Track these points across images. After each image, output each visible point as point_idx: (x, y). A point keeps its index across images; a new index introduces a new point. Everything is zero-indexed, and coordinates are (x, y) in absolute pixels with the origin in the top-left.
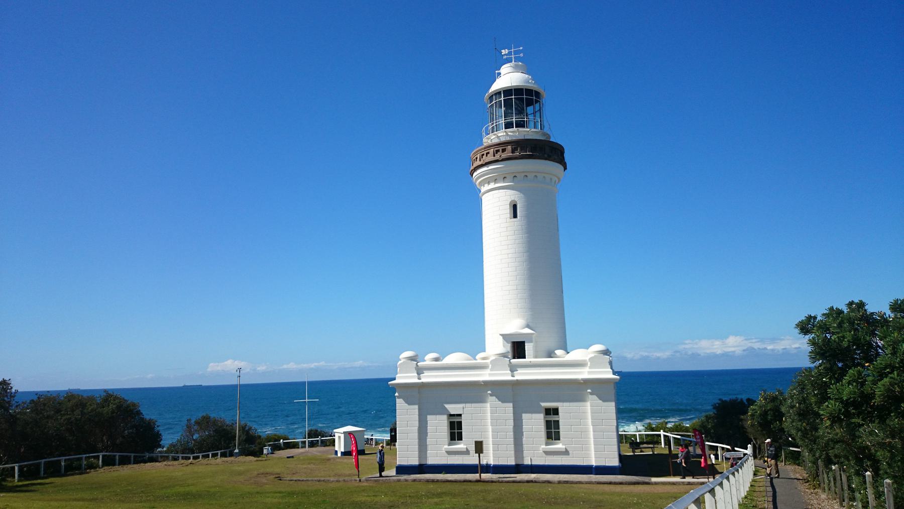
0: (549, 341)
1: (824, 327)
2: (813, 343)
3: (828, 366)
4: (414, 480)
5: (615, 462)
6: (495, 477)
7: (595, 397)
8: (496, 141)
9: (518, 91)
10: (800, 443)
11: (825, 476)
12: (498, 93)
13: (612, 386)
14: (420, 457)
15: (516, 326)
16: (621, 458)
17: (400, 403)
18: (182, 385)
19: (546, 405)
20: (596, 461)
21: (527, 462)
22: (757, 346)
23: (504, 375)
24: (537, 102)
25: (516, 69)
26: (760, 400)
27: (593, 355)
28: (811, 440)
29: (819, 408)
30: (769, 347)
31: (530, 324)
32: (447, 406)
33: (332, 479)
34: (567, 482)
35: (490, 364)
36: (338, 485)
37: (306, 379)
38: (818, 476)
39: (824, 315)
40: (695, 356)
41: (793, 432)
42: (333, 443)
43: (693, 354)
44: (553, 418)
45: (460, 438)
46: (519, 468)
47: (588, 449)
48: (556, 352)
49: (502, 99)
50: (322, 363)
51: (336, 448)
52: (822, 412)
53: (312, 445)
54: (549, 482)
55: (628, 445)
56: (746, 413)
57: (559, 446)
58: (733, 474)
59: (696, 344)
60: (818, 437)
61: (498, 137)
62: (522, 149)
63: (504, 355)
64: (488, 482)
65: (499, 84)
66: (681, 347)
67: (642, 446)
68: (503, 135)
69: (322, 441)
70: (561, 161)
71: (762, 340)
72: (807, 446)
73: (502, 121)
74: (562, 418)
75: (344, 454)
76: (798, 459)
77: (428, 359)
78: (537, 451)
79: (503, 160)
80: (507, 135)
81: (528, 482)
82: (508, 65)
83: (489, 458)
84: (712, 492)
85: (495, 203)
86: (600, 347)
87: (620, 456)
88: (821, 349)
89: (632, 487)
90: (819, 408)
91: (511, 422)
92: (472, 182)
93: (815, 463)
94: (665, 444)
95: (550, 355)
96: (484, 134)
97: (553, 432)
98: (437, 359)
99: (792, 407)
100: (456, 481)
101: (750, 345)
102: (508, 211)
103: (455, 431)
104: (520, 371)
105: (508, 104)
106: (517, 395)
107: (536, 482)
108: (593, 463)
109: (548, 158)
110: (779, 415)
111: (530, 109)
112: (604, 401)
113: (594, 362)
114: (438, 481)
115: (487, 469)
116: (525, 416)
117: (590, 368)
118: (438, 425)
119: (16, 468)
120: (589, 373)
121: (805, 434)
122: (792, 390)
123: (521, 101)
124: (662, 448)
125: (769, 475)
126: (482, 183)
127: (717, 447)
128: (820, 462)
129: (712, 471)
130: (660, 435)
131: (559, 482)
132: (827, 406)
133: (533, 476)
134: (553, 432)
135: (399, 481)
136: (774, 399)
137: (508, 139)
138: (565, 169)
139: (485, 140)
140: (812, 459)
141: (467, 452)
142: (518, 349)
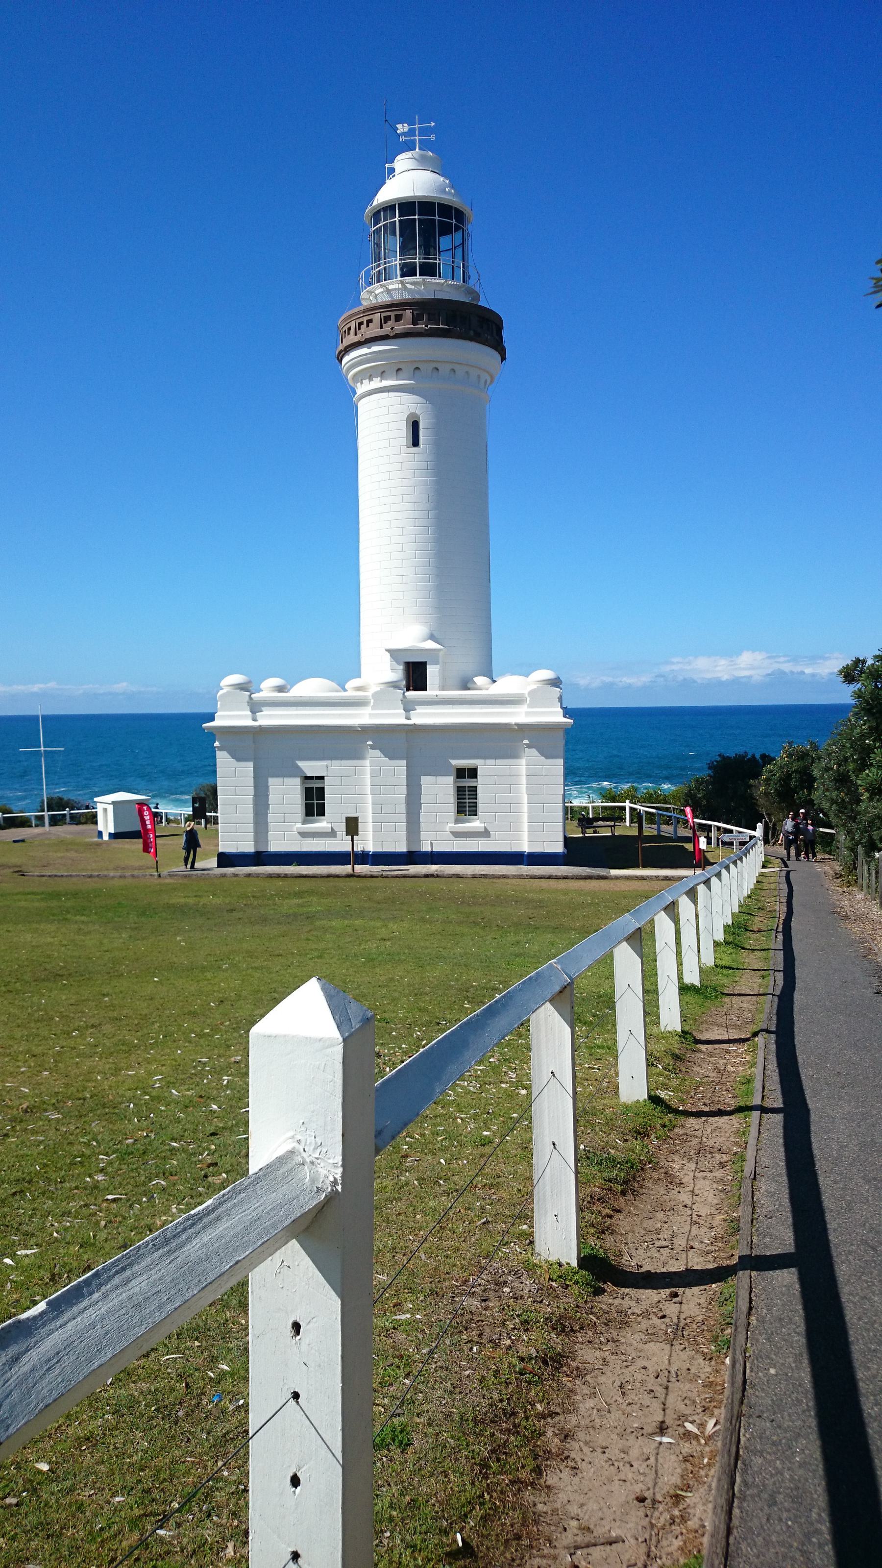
0: (464, 662)
1: (875, 674)
2: (859, 695)
3: (874, 724)
4: (249, 875)
5: (558, 847)
6: (376, 869)
7: (534, 751)
8: (384, 299)
9: (425, 206)
10: (834, 820)
11: (866, 867)
12: (389, 208)
13: (561, 734)
14: (256, 841)
15: (413, 636)
16: (567, 841)
17: (223, 758)
19: (459, 763)
20: (529, 846)
21: (426, 847)
22: (787, 667)
23: (395, 717)
24: (457, 228)
25: (423, 163)
26: (781, 757)
27: (535, 687)
28: (850, 817)
29: (857, 776)
30: (808, 671)
31: (435, 633)
32: (301, 764)
33: (112, 874)
34: (485, 876)
35: (371, 695)
36: (122, 882)
37: (39, 710)
38: (855, 868)
39: (876, 657)
40: (687, 684)
41: (826, 805)
42: (93, 819)
43: (685, 679)
44: (468, 782)
45: (322, 813)
46: (412, 857)
47: (519, 830)
48: (476, 679)
49: (397, 219)
50: (52, 685)
51: (100, 827)
52: (859, 782)
53: (55, 821)
54: (458, 876)
55: (576, 822)
56: (757, 775)
57: (475, 824)
58: (735, 863)
59: (689, 663)
60: (859, 813)
61: (388, 291)
62: (432, 319)
63: (394, 685)
64: (365, 877)
65: (391, 191)
66: (666, 669)
67: (595, 824)
68: (396, 288)
69: (72, 816)
70: (498, 346)
71: (795, 660)
72: (844, 825)
73: (396, 262)
74: (483, 783)
75: (114, 836)
76: (829, 844)
77: (267, 689)
78: (441, 831)
79: (397, 336)
80: (405, 288)
81: (427, 876)
82: (408, 154)
83: (367, 842)
84: (692, 894)
85: (381, 416)
86: (547, 674)
87: (566, 839)
88: (868, 703)
89: (582, 883)
90: (857, 776)
91: (404, 790)
92: (340, 372)
93: (853, 850)
94: (632, 821)
95: (466, 684)
96: (362, 282)
97: (466, 803)
98: (281, 689)
99: (828, 769)
100: (314, 876)
101: (776, 666)
102: (403, 433)
103: (314, 801)
104: (420, 710)
105: (407, 228)
106: (412, 747)
107: (438, 876)
108: (526, 847)
109: (476, 338)
110: (808, 781)
111: (445, 242)
112: (547, 757)
113: (536, 697)
114: (286, 876)
115: (364, 858)
116: (425, 780)
117: (529, 706)
118: (287, 794)
120: (528, 714)
121: (842, 806)
122: (830, 746)
123: (427, 226)
124: (627, 828)
126: (360, 377)
127: (710, 826)
128: (860, 850)
129: (699, 860)
130: (624, 808)
131: (474, 877)
132: (868, 775)
133: (433, 868)
134: (466, 803)
135: (224, 876)
136: (803, 756)
137: (407, 296)
138: (503, 358)
139: (364, 295)
140: (849, 844)
141: (332, 834)
142: (415, 675)
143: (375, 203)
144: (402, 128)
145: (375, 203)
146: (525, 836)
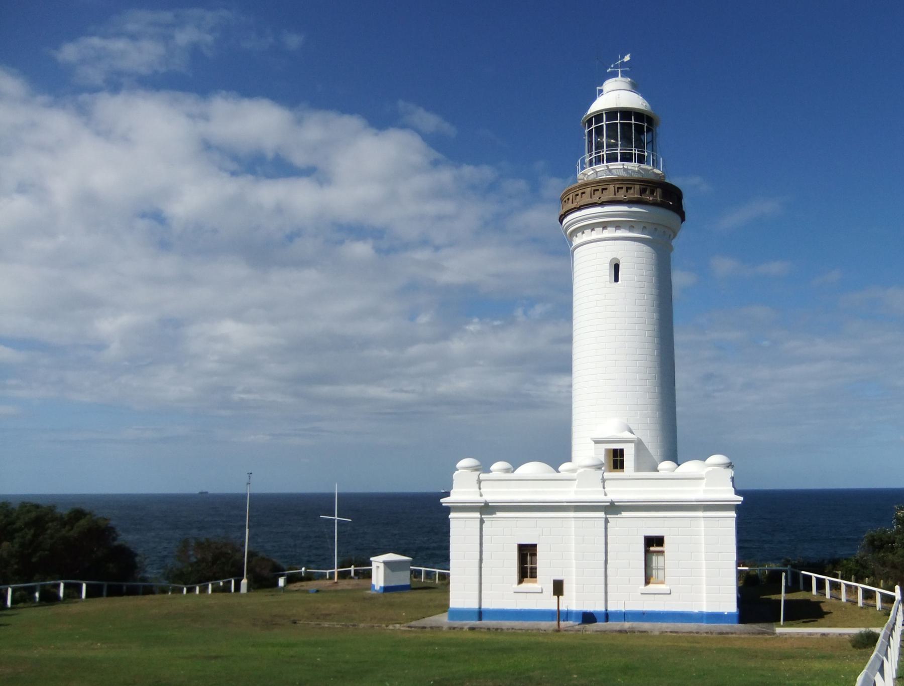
9: (626, 113)
12: (598, 117)
18: (197, 492)
42: (368, 575)
63: (598, 467)
65: (600, 105)
75: (386, 589)
78: (629, 595)
96: (579, 168)
102: (608, 272)
115: (568, 615)
119: (84, 586)
123: (632, 129)
125: (791, 669)
138: (683, 219)
139: (580, 175)
142: (617, 459)
143: (589, 113)
145: (589, 113)
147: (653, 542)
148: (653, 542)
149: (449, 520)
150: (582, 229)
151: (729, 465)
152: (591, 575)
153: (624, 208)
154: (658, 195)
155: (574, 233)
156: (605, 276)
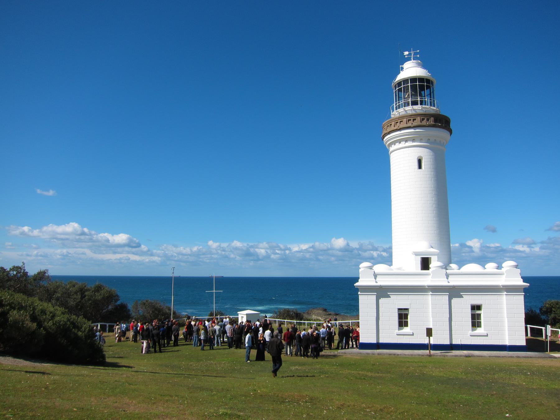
5: (524, 343)
15: (425, 246)
27: (508, 268)
40: (285, 260)
45: (406, 325)
61: (406, 111)
65: (401, 76)
78: (464, 335)
97: (476, 322)
103: (403, 318)
105: (414, 88)
108: (507, 343)
123: (420, 86)
134: (476, 322)
139: (392, 116)
142: (425, 264)
144: (406, 53)
146: (507, 337)
147: (476, 308)
148: (476, 308)
149: (358, 295)
150: (394, 143)
151: (516, 267)
152: (433, 321)
153: (412, 130)
154: (432, 121)
155: (390, 145)
156: (407, 164)
